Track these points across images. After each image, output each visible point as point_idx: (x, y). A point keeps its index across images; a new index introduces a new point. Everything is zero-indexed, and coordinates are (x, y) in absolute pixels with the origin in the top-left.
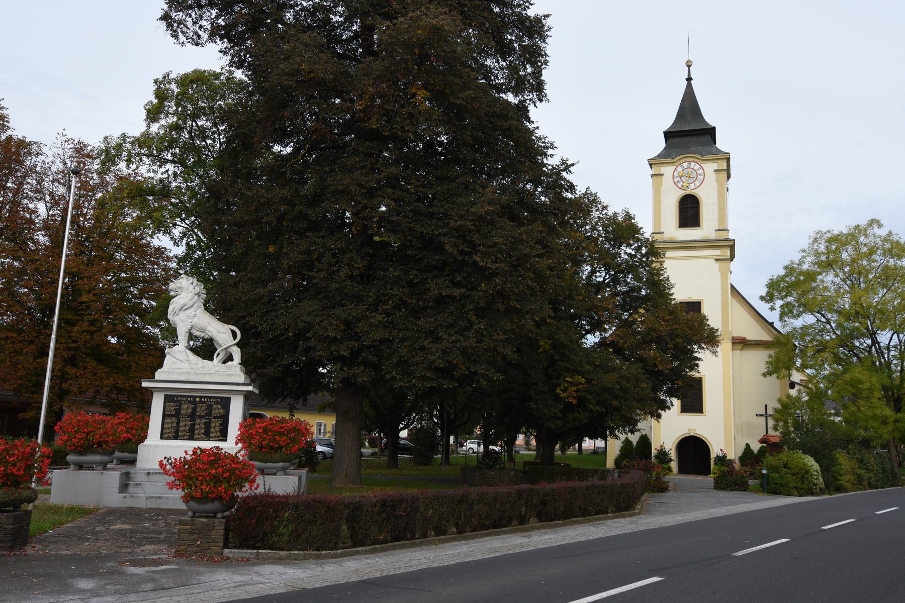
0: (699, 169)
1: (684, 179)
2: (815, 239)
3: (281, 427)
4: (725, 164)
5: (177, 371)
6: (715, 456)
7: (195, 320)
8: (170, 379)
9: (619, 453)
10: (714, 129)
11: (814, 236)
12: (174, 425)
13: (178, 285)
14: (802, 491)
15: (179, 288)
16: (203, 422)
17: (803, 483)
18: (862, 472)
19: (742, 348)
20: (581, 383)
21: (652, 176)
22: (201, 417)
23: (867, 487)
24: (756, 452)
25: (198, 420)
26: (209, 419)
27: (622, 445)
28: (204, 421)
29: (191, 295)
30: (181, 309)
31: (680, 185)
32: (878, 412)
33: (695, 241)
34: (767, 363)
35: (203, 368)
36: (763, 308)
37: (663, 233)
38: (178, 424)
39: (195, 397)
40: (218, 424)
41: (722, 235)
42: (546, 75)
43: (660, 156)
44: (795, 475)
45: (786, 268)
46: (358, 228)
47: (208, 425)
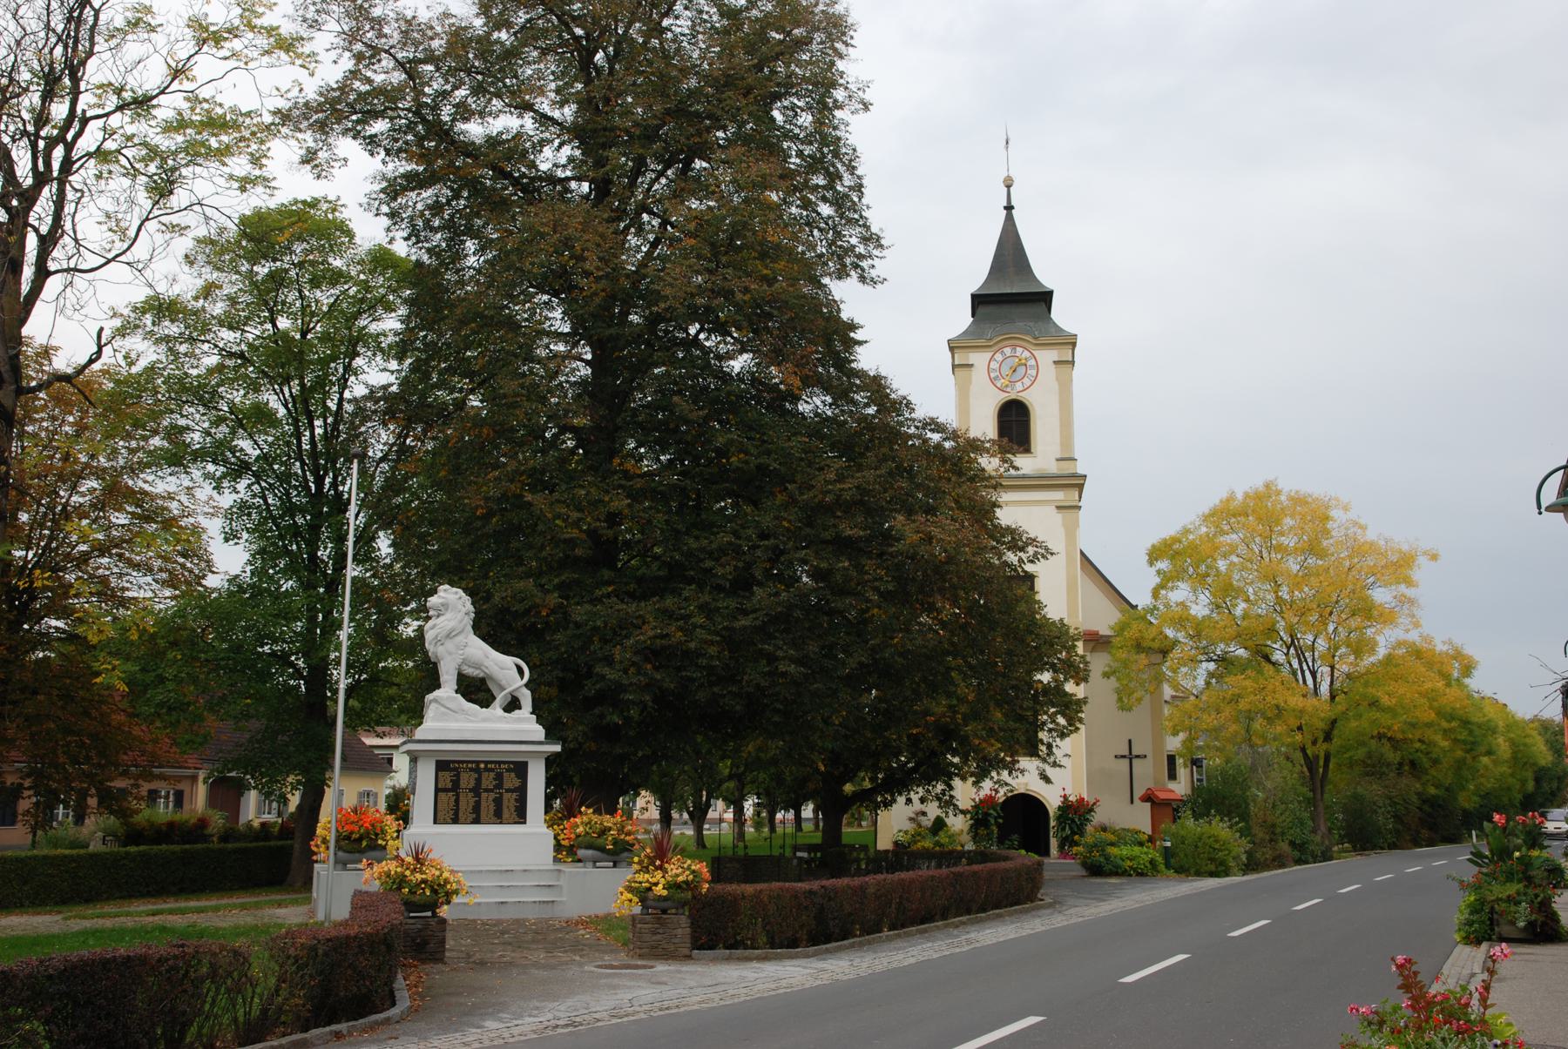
12: (452, 803)
16: (491, 799)
22: (487, 790)
25: (484, 795)
28: (492, 796)
29: (460, 616)
38: (457, 801)
40: (513, 801)
41: (1067, 468)
47: (498, 802)
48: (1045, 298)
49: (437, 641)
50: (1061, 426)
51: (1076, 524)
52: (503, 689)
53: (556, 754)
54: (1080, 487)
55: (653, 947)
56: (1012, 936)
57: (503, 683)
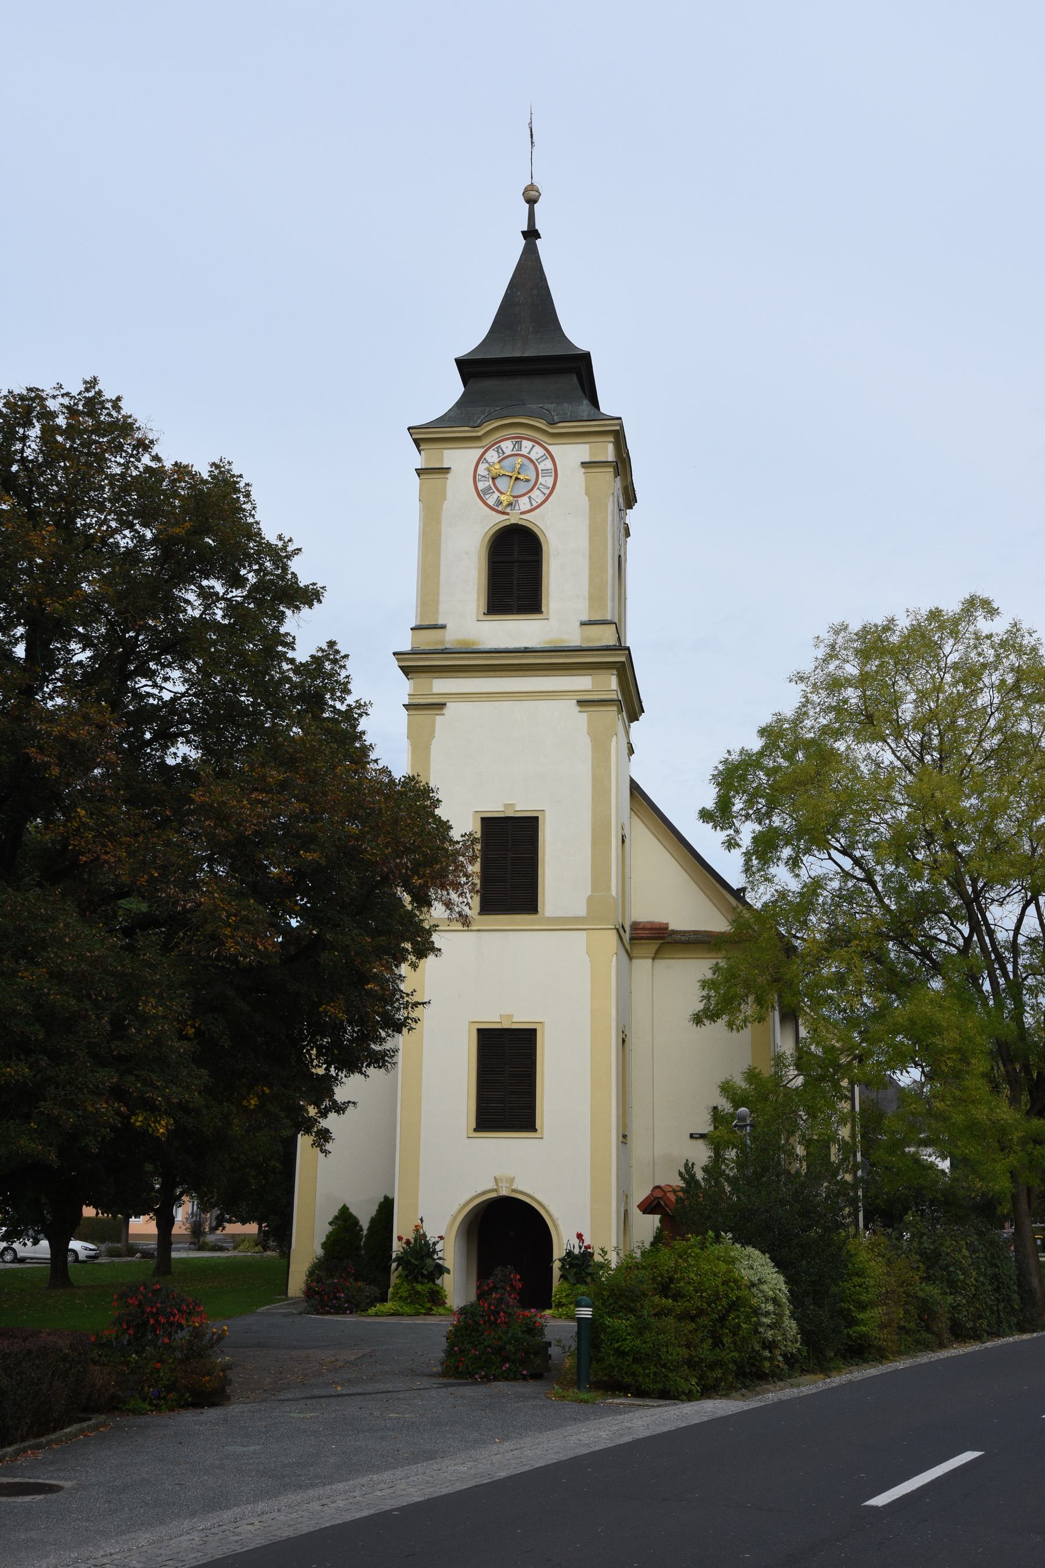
0: (542, 459)
1: (502, 483)
2: (833, 647)
4: (611, 447)
10: (589, 354)
14: (718, 1373)
17: (717, 1343)
18: (933, 1291)
19: (657, 952)
21: (419, 472)
23: (947, 1335)
27: (330, 1229)
31: (491, 501)
32: (980, 1113)
33: (526, 651)
37: (443, 627)
44: (693, 1319)
45: (763, 732)
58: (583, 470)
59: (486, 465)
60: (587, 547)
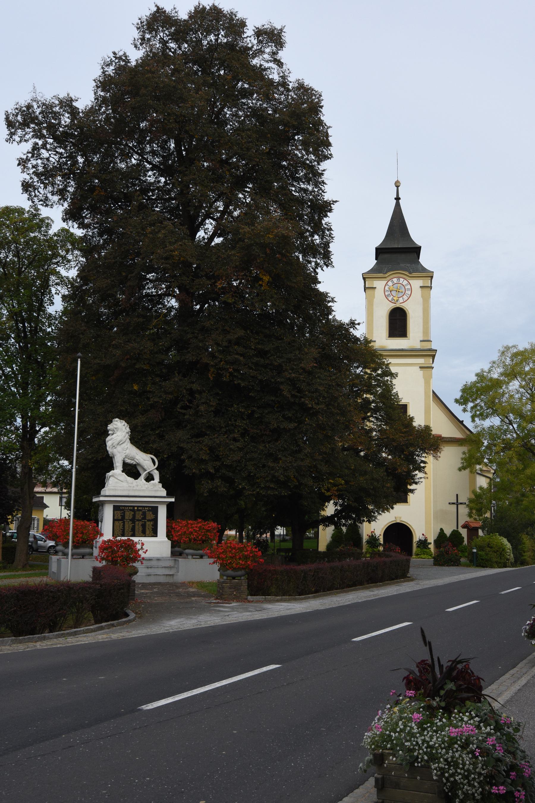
1: (394, 293)
3: (209, 527)
5: (120, 488)
6: (418, 540)
7: (128, 451)
8: (117, 494)
9: (331, 539)
10: (420, 248)
11: (502, 349)
13: (115, 426)
15: (116, 428)
16: (140, 524)
20: (341, 484)
22: (138, 520)
24: (448, 535)
25: (137, 523)
26: (144, 522)
27: (333, 532)
28: (141, 523)
30: (118, 444)
31: (390, 299)
33: (402, 350)
34: (462, 459)
35: (137, 486)
36: (457, 410)
38: (124, 526)
39: (134, 507)
40: (151, 526)
41: (426, 346)
42: (332, 247)
43: (372, 271)
45: (477, 375)
46: (213, 375)
47: (144, 526)
48: (417, 250)
49: (113, 447)
50: (423, 322)
51: (431, 377)
52: (146, 470)
53: (171, 503)
54: (433, 357)
55: (230, 595)
56: (395, 594)
57: (145, 467)
58: (420, 289)
59: (388, 287)
60: (422, 315)
